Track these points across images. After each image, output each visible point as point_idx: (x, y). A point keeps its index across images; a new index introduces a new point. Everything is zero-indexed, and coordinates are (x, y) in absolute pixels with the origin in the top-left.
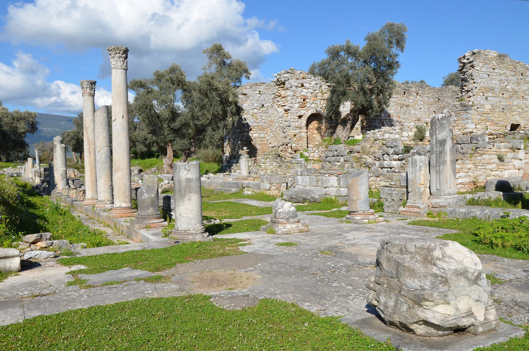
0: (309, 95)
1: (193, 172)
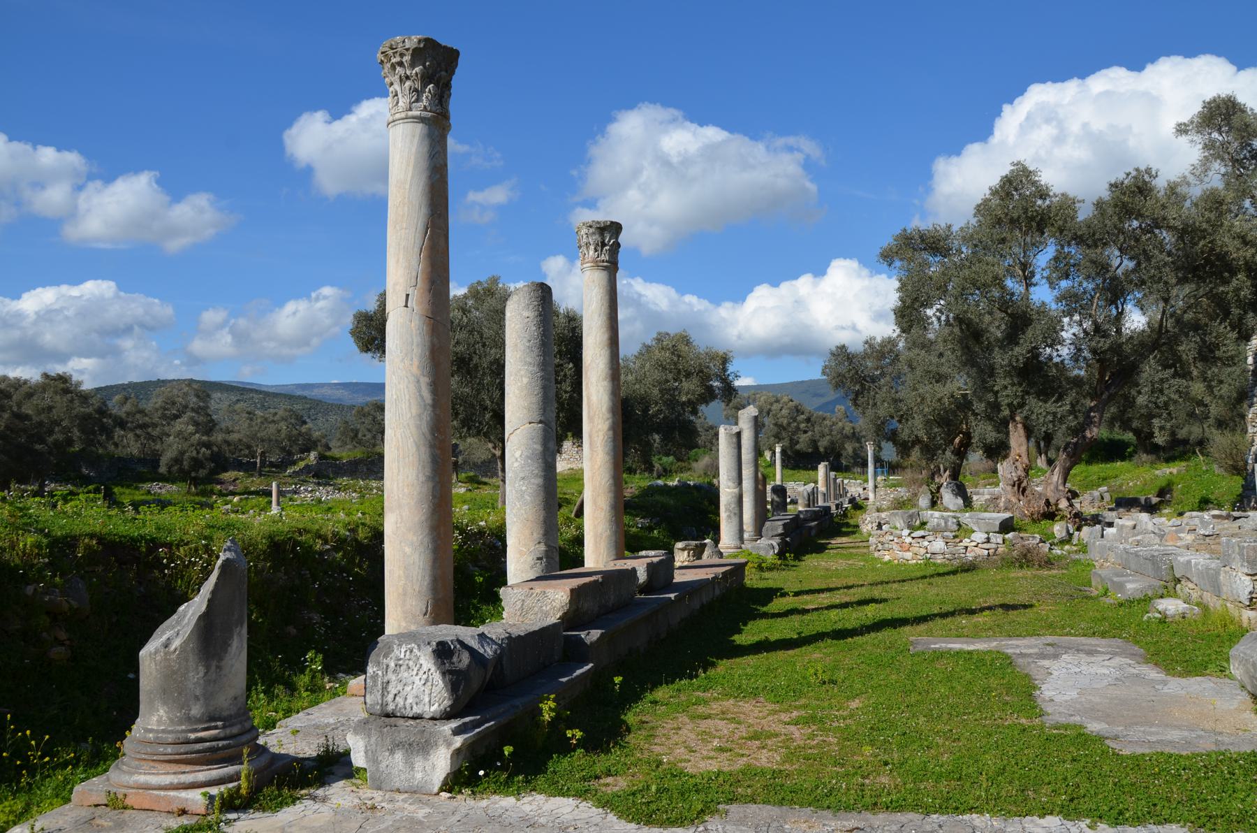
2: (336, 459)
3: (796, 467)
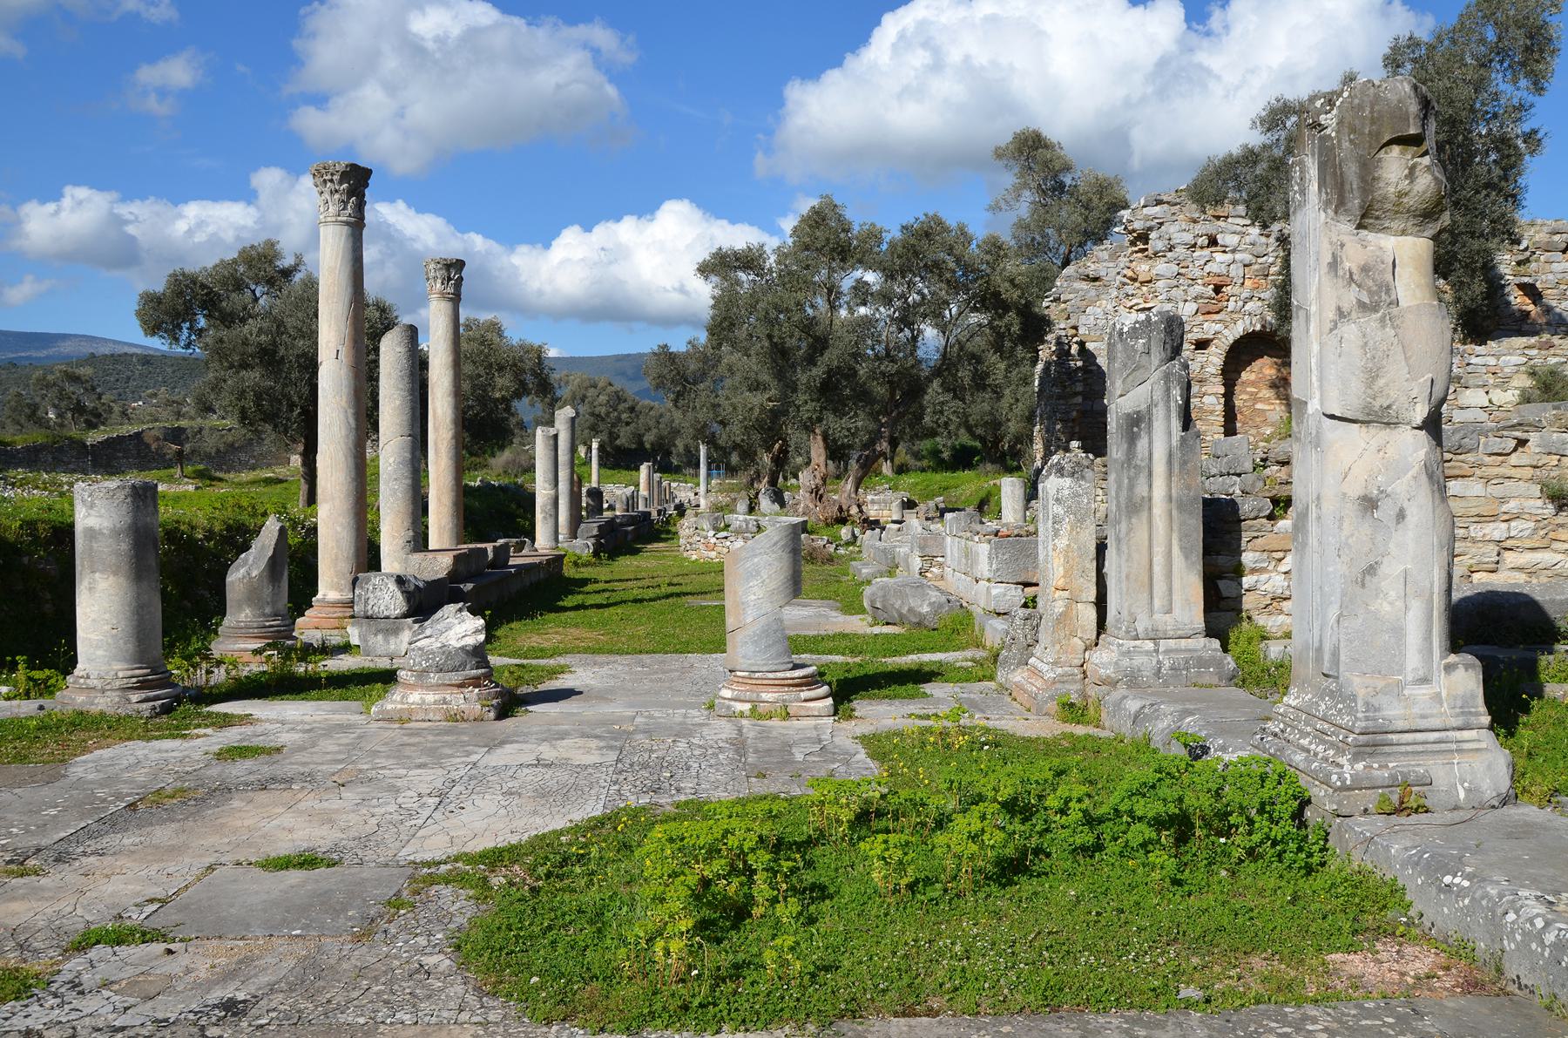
0: (1236, 271)
1: (103, 511)
2: (7, 444)
3: (616, 466)
